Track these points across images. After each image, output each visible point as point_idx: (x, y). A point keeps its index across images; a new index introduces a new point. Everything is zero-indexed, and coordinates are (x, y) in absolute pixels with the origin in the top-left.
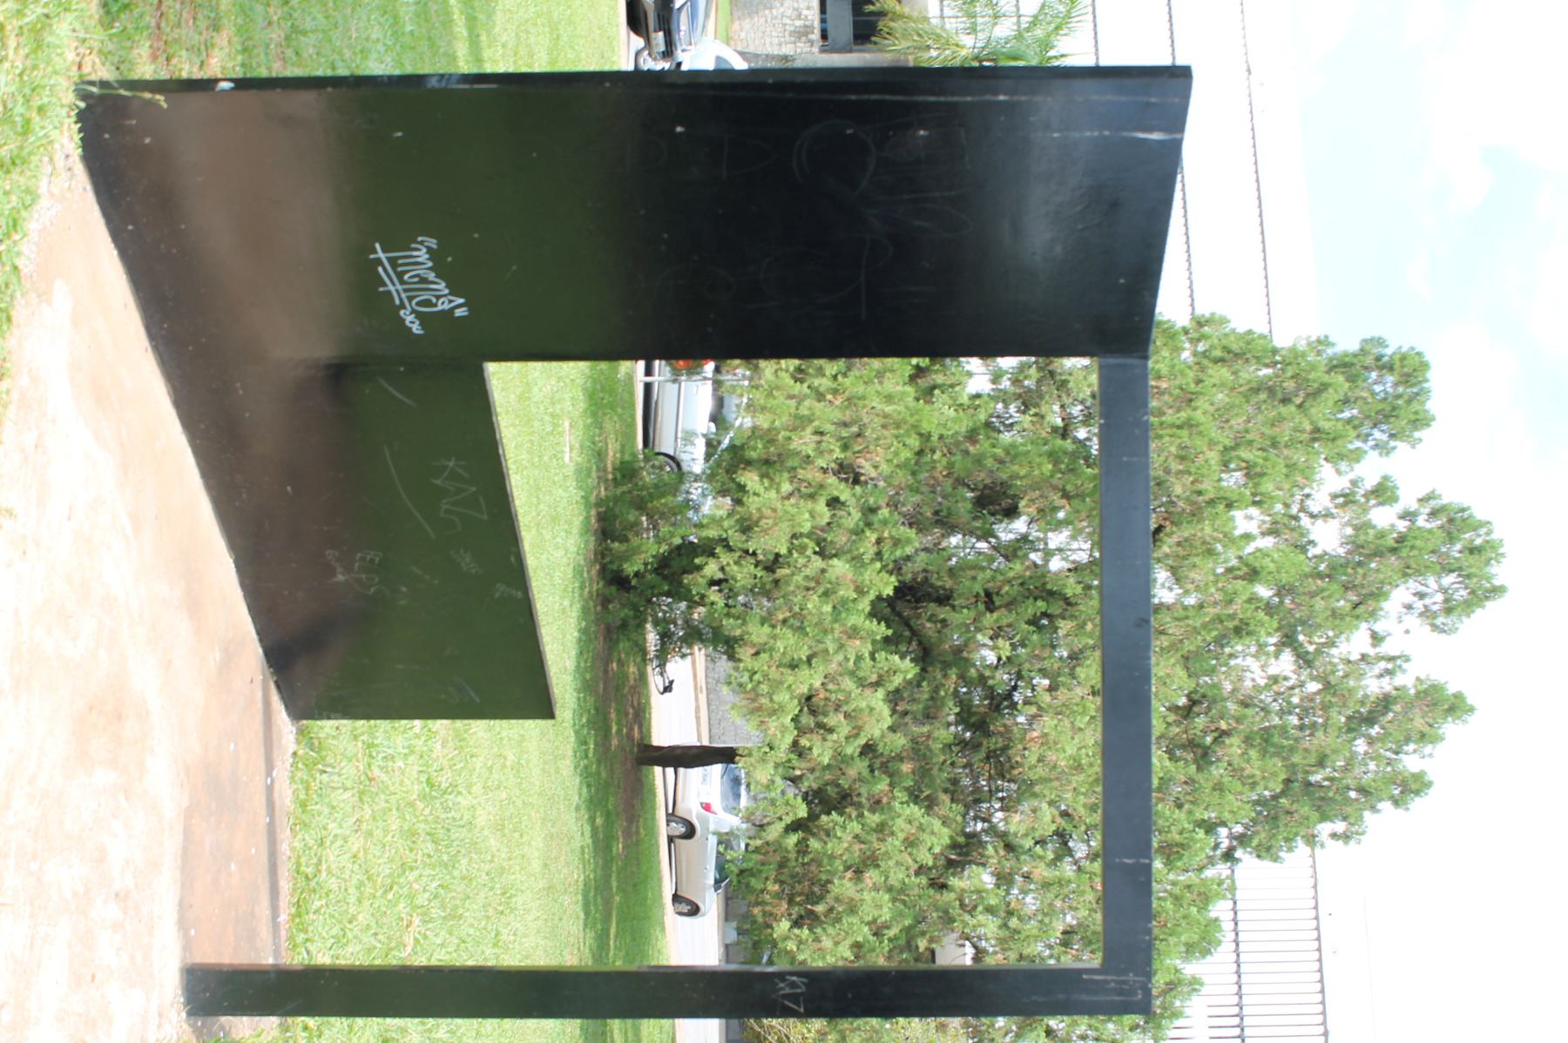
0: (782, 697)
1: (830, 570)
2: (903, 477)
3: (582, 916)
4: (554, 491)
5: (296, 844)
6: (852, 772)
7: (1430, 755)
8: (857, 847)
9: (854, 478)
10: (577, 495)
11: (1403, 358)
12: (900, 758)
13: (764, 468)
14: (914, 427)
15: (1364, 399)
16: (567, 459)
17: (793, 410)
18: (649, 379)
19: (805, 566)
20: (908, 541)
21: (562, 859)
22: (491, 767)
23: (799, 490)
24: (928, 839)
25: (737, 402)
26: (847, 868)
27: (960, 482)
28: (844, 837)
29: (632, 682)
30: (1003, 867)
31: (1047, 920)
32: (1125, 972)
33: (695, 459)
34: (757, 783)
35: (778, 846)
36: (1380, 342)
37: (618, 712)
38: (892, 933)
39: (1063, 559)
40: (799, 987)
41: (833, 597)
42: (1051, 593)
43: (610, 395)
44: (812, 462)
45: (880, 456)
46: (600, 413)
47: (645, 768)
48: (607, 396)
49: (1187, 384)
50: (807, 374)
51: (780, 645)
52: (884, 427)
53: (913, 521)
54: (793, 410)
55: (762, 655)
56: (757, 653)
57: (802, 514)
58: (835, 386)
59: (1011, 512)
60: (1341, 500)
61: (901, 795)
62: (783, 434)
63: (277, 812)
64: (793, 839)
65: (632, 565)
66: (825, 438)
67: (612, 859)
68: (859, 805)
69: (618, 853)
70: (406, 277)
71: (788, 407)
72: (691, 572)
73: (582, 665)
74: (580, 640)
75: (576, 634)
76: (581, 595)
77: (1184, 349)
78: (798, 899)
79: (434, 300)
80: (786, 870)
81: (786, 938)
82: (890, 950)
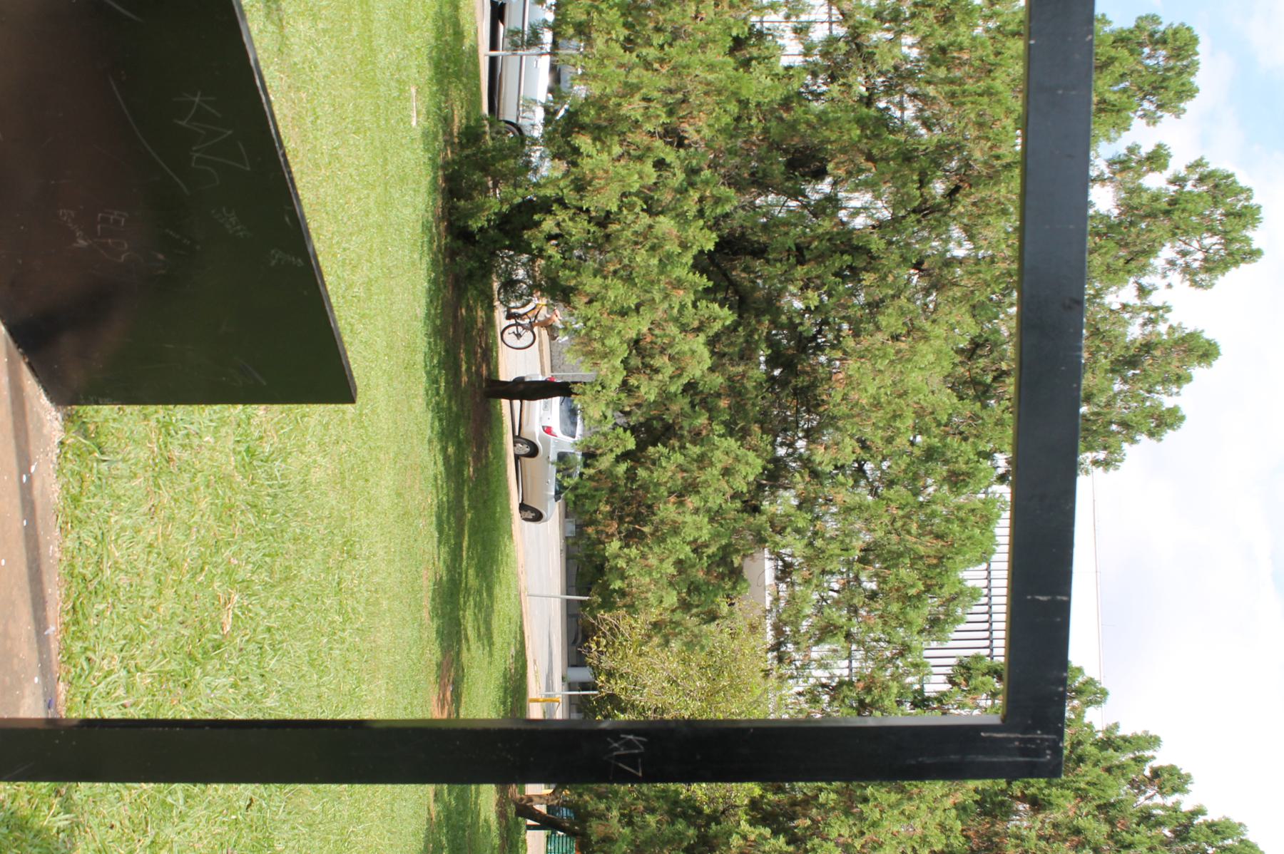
0: (613, 341)
1: (657, 226)
3: (436, 535)
5: (68, 544)
6: (675, 408)
7: (1178, 393)
8: (679, 476)
10: (424, 157)
11: (1175, 32)
14: (734, 93)
15: (1139, 72)
16: (414, 123)
18: (494, 53)
19: (634, 222)
20: (728, 200)
21: (417, 487)
22: (327, 423)
24: (743, 469)
26: (671, 493)
27: (775, 146)
28: (668, 466)
29: (480, 325)
30: (809, 493)
31: (847, 540)
33: (535, 122)
34: (590, 418)
35: (609, 474)
36: (1154, 19)
37: (467, 352)
38: (710, 551)
39: (869, 217)
41: (660, 251)
42: (857, 248)
43: (455, 65)
44: (640, 127)
45: (702, 121)
46: (446, 81)
47: (492, 400)
48: (452, 66)
49: (987, 56)
50: (636, 44)
51: (611, 294)
52: (706, 94)
53: (733, 182)
54: (622, 78)
55: (595, 303)
56: (590, 302)
57: (630, 175)
58: (662, 55)
59: (820, 174)
60: (1117, 167)
61: (720, 429)
62: (614, 100)
63: (39, 512)
64: (622, 468)
65: (476, 222)
66: (652, 104)
67: (464, 481)
69: (469, 476)
72: (529, 228)
73: (433, 312)
74: (430, 289)
76: (430, 249)
77: (978, 26)
78: (627, 520)
81: (618, 556)
82: (709, 565)
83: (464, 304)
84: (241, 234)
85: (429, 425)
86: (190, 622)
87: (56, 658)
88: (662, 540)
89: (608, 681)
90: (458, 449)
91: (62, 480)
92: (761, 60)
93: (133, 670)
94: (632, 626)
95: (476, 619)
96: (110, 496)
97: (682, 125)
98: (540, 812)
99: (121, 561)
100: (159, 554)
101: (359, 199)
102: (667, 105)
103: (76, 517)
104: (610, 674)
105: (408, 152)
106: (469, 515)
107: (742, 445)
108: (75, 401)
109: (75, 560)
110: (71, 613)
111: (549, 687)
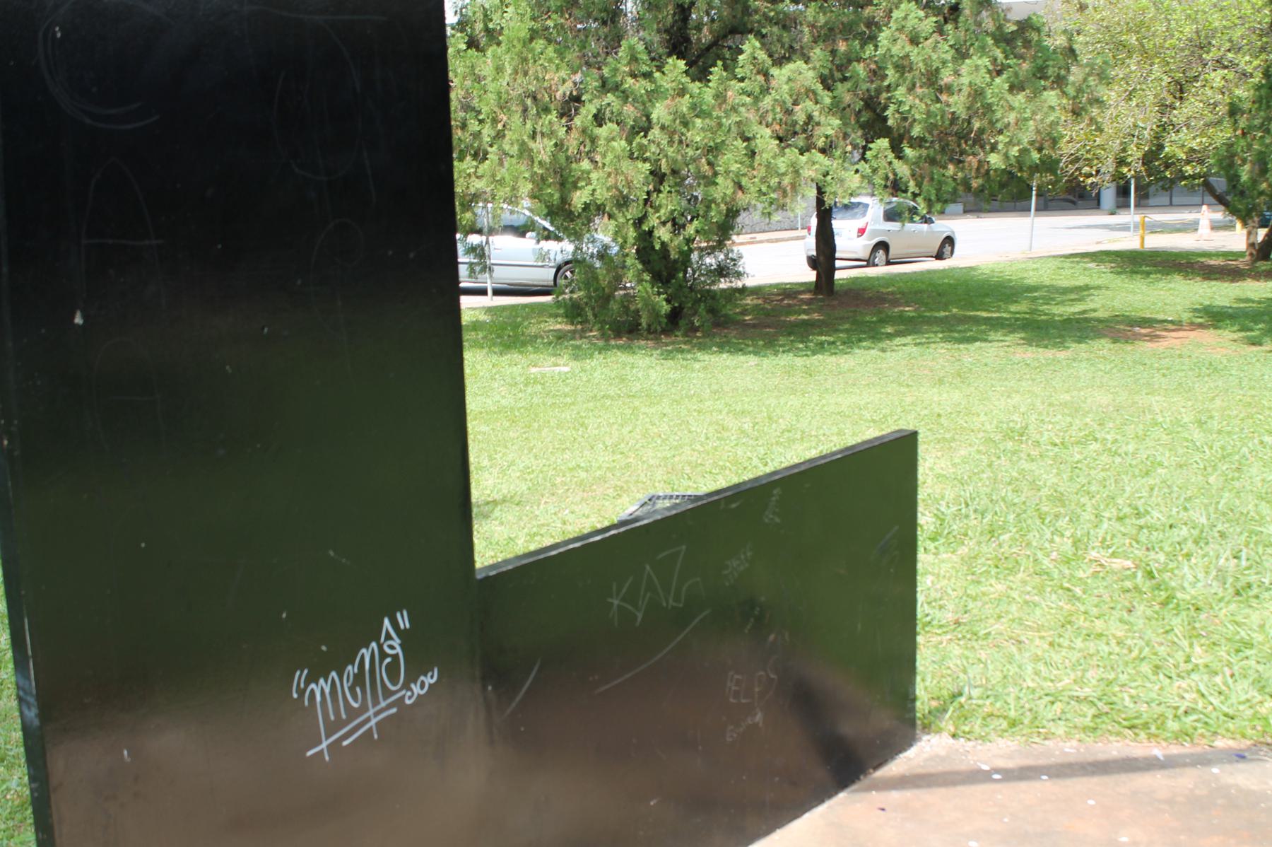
0: (782, 164)
1: (662, 121)
3: (978, 344)
4: (596, 381)
6: (847, 98)
8: (919, 91)
10: (598, 359)
12: (833, 52)
13: (568, 186)
16: (566, 369)
17: (514, 161)
18: (490, 292)
19: (658, 145)
20: (632, 48)
21: (930, 364)
24: (911, 22)
25: (508, 213)
26: (938, 100)
28: (909, 103)
29: (760, 302)
33: (562, 249)
37: (788, 314)
43: (506, 329)
44: (562, 141)
45: (553, 77)
47: (836, 288)
48: (507, 332)
52: (526, 74)
53: (614, 41)
55: (743, 183)
56: (740, 187)
61: (869, 49)
64: (908, 151)
66: (539, 129)
67: (920, 316)
68: (879, 91)
70: (355, 705)
73: (751, 349)
75: (725, 356)
76: (689, 351)
79: (388, 660)
80: (938, 157)
81: (1006, 156)
83: (740, 317)
84: (749, 554)
85: (866, 352)
86: (1127, 604)
87: (1187, 748)
88: (988, 108)
89: (1129, 164)
90: (887, 323)
91: (993, 736)
92: (487, 18)
93: (1190, 666)
94: (1072, 138)
95: (1062, 303)
96: (1005, 687)
97: (558, 97)
98: (1267, 235)
99: (1073, 676)
100: (1060, 636)
101: (653, 424)
102: (538, 114)
103: (1032, 722)
104: (1121, 162)
105: (596, 375)
106: (955, 310)
107: (886, 25)
108: (912, 723)
109: (1078, 725)
110: (1137, 731)
111: (1125, 228)
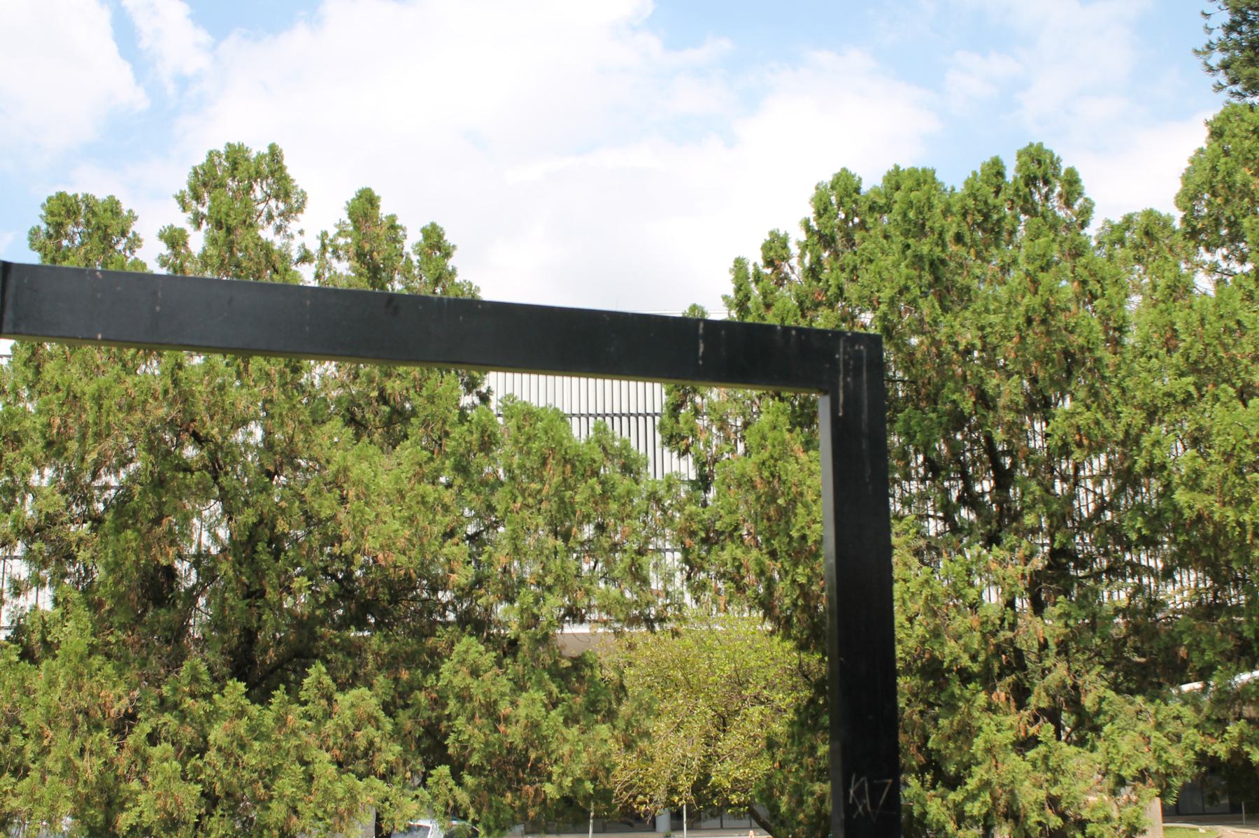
0: (339, 789)
2: (132, 674)
6: (409, 725)
8: (478, 721)
9: (128, 720)
11: (51, 213)
12: (396, 680)
14: (82, 659)
17: (56, 779)
20: (194, 668)
23: (139, 773)
24: (472, 656)
28: (469, 733)
32: (834, 362)
35: (474, 793)
36: (34, 233)
38: (555, 690)
40: (862, 785)
41: (246, 739)
42: (251, 537)
45: (109, 693)
49: (58, 399)
50: (21, 765)
51: (289, 791)
52: (80, 689)
55: (299, 808)
59: (170, 572)
61: (431, 679)
64: (469, 780)
66: (88, 747)
71: (53, 783)
77: (25, 408)
80: (496, 786)
81: (560, 786)
